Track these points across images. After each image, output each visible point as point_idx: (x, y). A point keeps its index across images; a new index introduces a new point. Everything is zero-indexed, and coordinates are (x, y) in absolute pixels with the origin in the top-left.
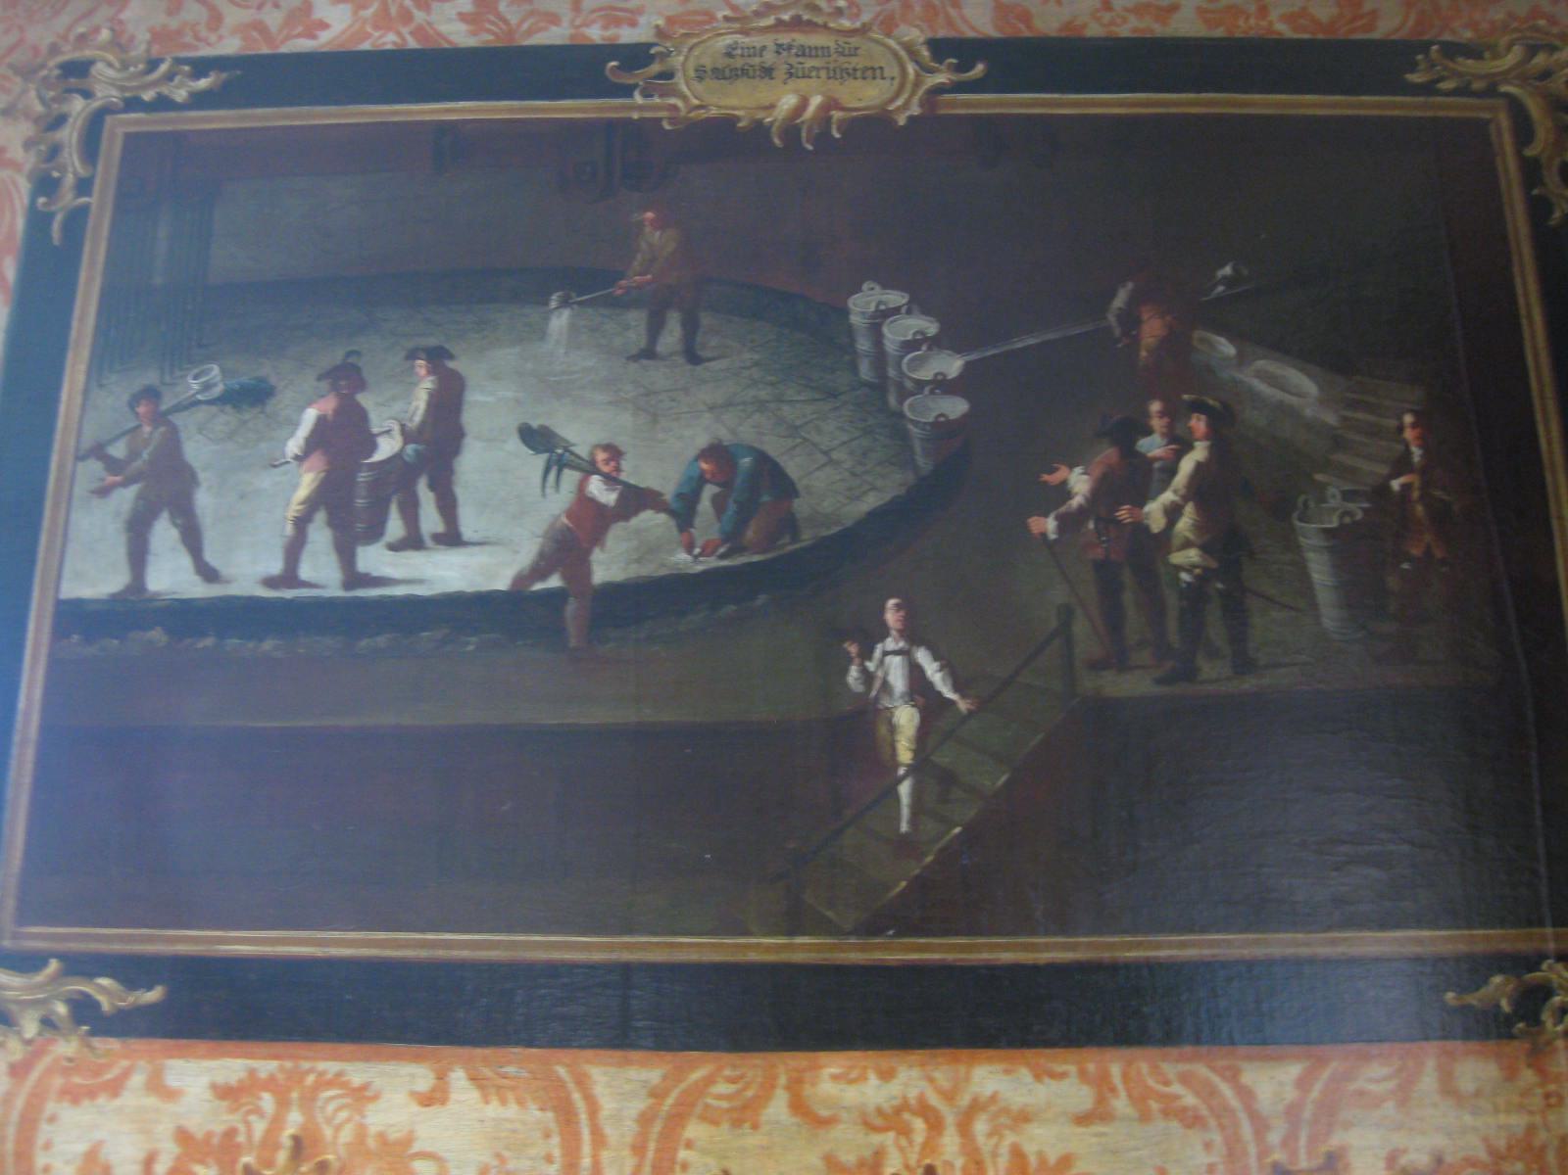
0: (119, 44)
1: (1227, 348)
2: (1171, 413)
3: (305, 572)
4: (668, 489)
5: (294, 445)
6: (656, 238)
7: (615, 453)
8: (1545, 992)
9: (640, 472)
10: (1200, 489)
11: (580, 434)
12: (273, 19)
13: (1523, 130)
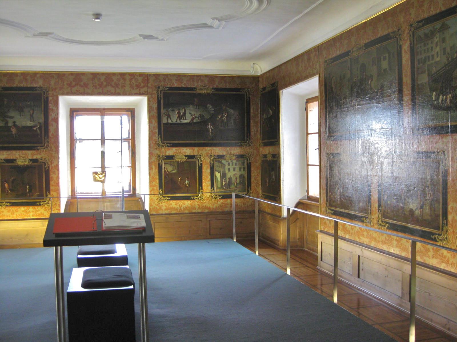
0: (161, 85)
1: (228, 109)
2: (225, 113)
3: (178, 121)
4: (197, 116)
5: (176, 114)
6: (196, 100)
7: (195, 114)
8: (242, 144)
9: (196, 116)
10: (226, 117)
11: (193, 113)
12: (171, 84)
13: (247, 94)
